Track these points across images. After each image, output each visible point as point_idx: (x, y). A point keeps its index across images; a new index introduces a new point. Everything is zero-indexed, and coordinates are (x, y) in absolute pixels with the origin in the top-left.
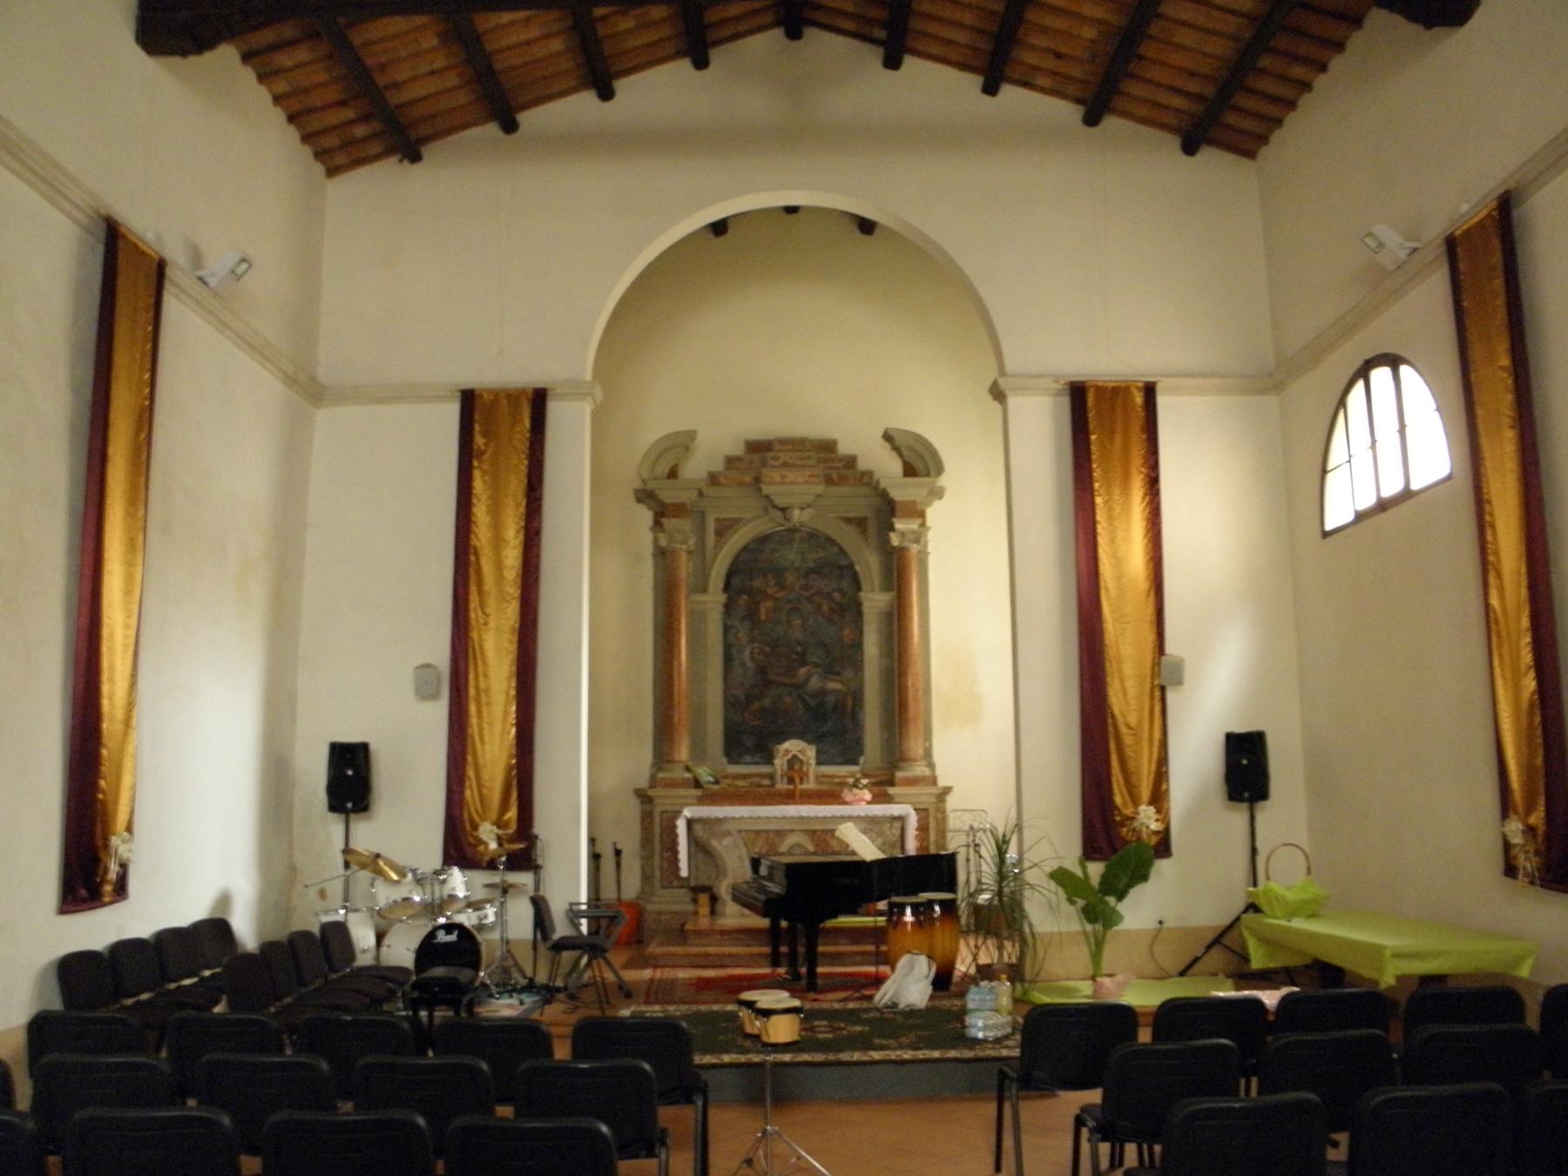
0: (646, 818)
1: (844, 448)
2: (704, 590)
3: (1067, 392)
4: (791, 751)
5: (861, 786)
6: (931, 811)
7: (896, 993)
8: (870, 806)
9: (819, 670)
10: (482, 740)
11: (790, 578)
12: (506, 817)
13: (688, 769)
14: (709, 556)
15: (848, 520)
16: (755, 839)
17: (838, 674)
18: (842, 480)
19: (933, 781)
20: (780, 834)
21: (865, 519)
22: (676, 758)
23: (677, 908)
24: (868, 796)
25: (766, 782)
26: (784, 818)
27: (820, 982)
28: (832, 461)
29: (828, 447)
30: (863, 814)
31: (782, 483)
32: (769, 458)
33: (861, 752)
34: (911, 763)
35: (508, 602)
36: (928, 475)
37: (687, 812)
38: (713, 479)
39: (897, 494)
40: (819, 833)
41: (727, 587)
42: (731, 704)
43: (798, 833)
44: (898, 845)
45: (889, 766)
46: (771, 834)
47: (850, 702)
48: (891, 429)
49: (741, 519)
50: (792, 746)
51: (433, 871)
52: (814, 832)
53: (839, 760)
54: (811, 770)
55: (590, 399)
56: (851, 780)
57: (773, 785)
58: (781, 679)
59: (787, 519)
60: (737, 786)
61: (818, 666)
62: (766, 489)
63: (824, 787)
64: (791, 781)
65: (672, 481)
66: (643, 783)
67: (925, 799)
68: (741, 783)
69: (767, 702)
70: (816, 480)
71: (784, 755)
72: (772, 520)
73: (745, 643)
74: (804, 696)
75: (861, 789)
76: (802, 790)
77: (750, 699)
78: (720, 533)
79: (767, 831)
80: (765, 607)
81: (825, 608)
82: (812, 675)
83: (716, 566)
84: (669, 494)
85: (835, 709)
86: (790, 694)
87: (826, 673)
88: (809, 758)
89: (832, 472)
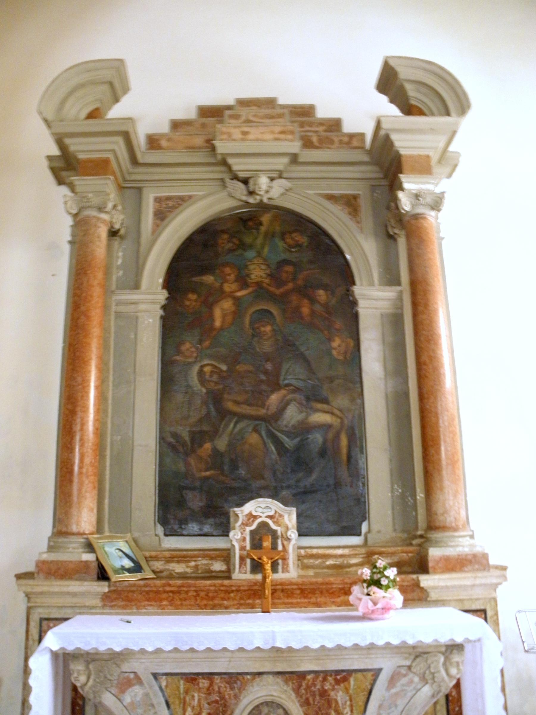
2: (137, 286)
4: (255, 517)
5: (384, 582)
9: (297, 396)
13: (90, 547)
14: (143, 249)
15: (331, 198)
16: (187, 692)
17: (325, 401)
28: (310, 124)
30: (395, 642)
33: (364, 516)
34: (447, 534)
40: (309, 677)
43: (270, 678)
45: (405, 535)
46: (217, 680)
47: (344, 441)
49: (190, 197)
52: (302, 675)
53: (332, 528)
54: (291, 549)
57: (227, 574)
61: (297, 390)
64: (257, 567)
68: (179, 568)
69: (222, 444)
71: (245, 524)
75: (388, 587)
76: (274, 584)
79: (210, 676)
82: (288, 404)
85: (323, 453)
86: (256, 430)
87: (308, 399)
88: (287, 529)
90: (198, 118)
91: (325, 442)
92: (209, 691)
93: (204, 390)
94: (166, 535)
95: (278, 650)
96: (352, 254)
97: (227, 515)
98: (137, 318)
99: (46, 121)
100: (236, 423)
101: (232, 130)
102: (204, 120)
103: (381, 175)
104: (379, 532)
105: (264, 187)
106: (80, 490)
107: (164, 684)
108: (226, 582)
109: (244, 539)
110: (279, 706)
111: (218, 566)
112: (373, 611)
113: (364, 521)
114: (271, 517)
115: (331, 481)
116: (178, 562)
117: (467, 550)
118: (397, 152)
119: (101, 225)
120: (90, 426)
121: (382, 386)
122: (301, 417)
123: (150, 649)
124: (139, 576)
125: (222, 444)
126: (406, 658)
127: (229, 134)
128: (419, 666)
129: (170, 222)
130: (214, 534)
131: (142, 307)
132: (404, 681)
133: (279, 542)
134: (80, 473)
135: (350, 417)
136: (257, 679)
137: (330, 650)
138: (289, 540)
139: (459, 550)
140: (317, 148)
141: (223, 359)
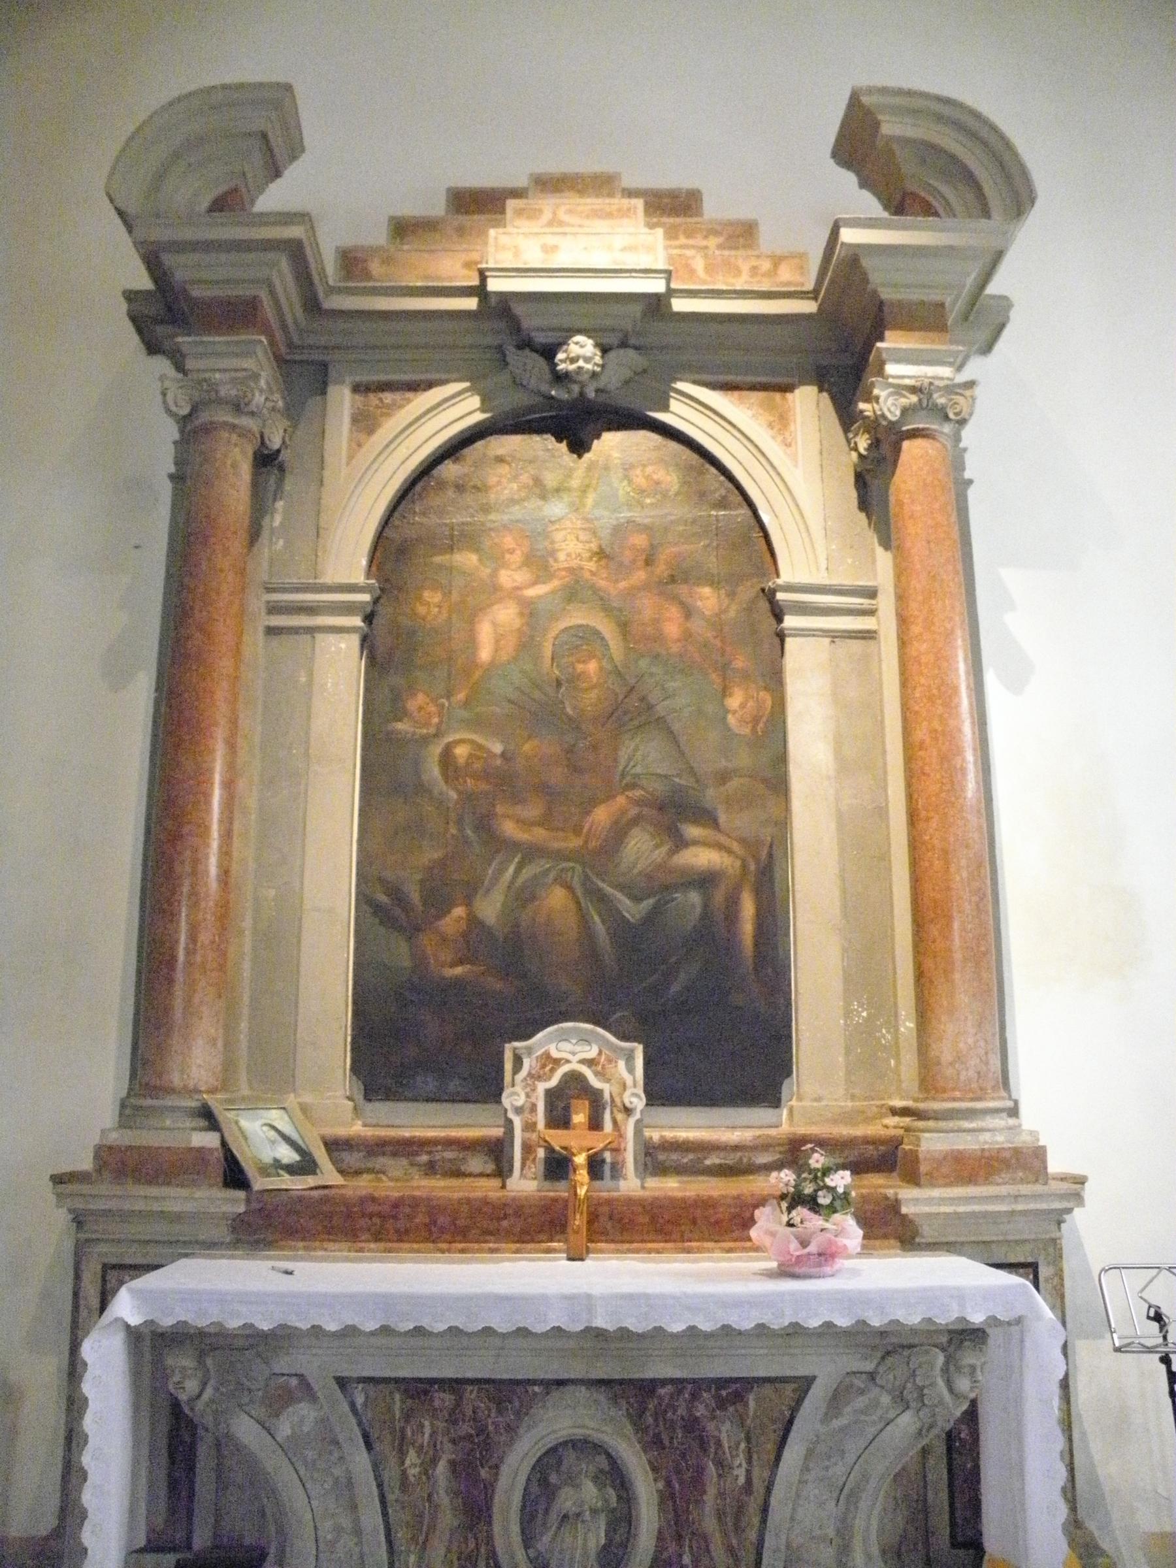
4: (557, 1062)
5: (824, 1199)
16: (407, 1416)
22: (176, 1080)
33: (783, 1068)
43: (582, 1392)
46: (471, 1393)
52: (648, 1387)
72: (517, 384)
75: (832, 1209)
79: (455, 1385)
90: (447, 212)
106: (188, 1001)
107: (360, 1400)
109: (533, 1108)
110: (598, 1448)
114: (590, 1063)
125: (490, 908)
132: (860, 1402)
136: (556, 1394)
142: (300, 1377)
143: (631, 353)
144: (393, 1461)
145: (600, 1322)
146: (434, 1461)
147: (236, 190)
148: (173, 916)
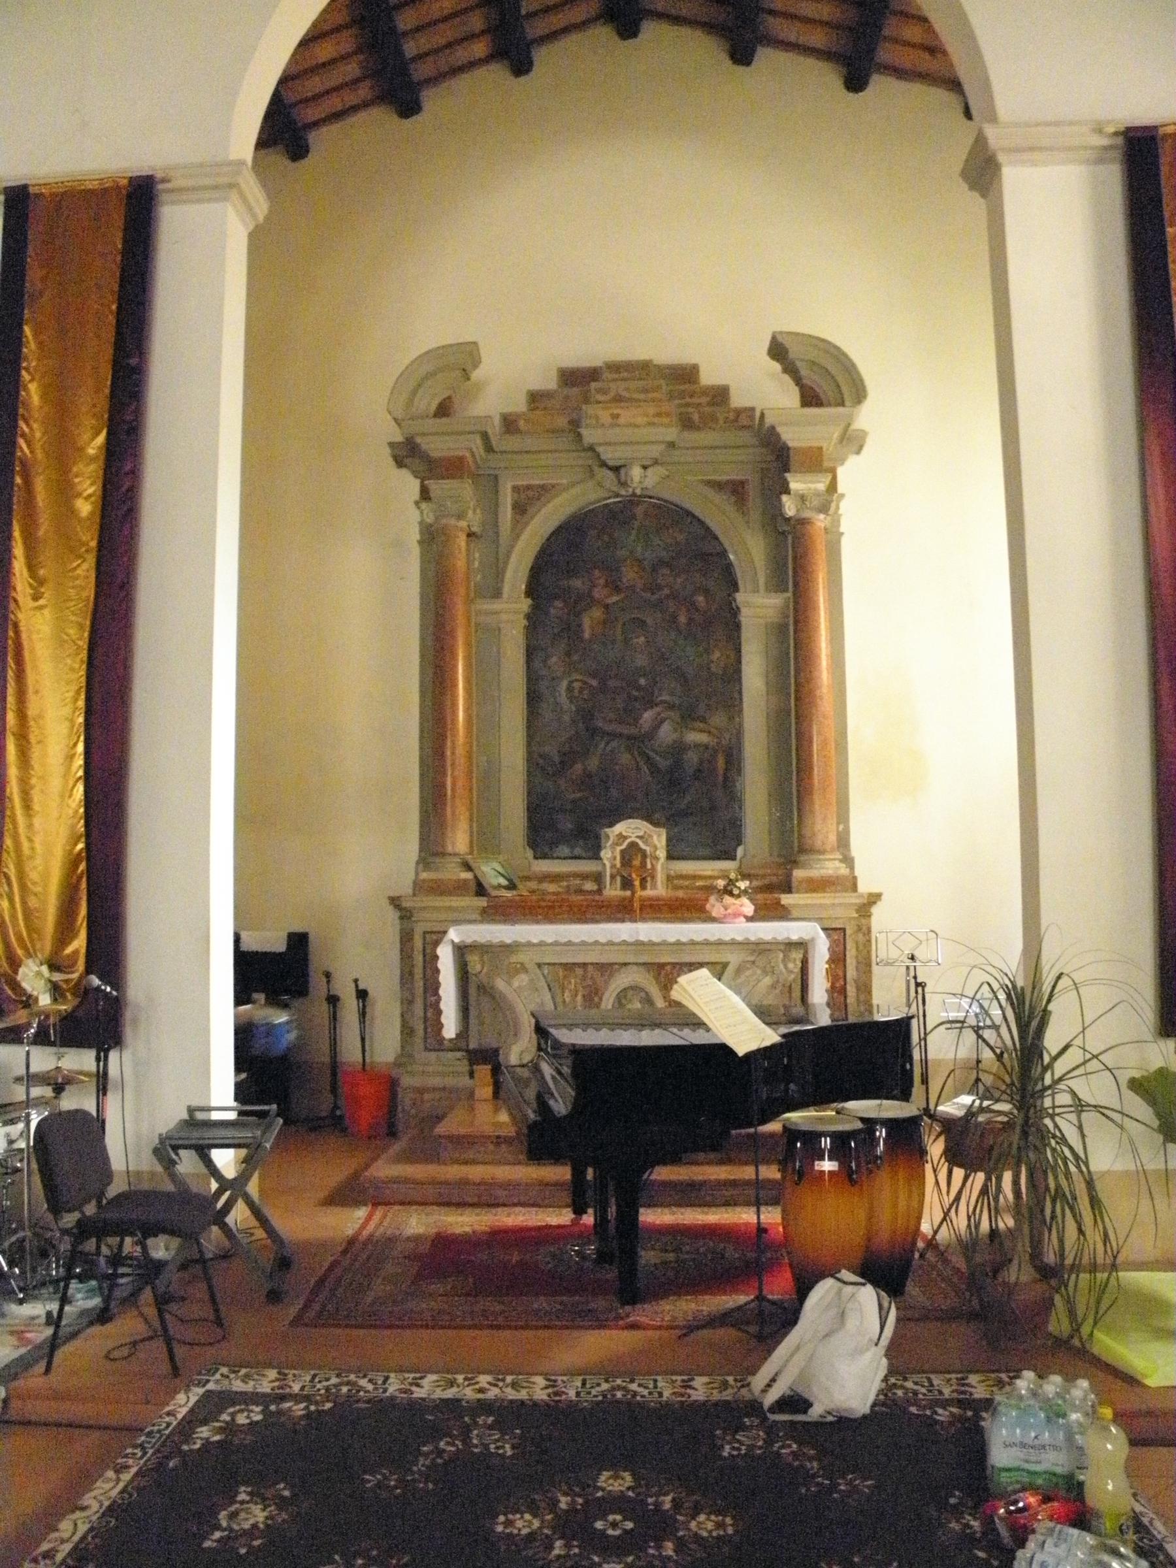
0: (406, 938)
1: (709, 377)
2: (497, 594)
3: (1117, 155)
4: (625, 838)
5: (736, 892)
6: (848, 932)
7: (803, 1375)
8: (751, 924)
10: (27, 806)
11: (629, 575)
12: (69, 950)
13: (468, 867)
14: (502, 550)
15: (719, 486)
16: (565, 977)
17: (703, 720)
18: (708, 422)
19: (852, 884)
20: (607, 969)
21: (742, 483)
23: (450, 1081)
24: (748, 908)
25: (589, 886)
26: (610, 943)
27: (648, 1257)
29: (685, 375)
30: (739, 938)
31: (613, 426)
32: (593, 391)
34: (812, 857)
35: (79, 557)
36: (842, 404)
37: (454, 935)
38: (510, 424)
39: (792, 436)
40: (668, 968)
41: (530, 592)
42: (536, 764)
43: (635, 968)
44: (797, 993)
46: (590, 968)
47: (721, 762)
48: (781, 332)
50: (629, 829)
51: (331, 970)
52: (661, 966)
53: (703, 852)
55: (234, 195)
56: (721, 883)
57: (599, 891)
58: (609, 728)
59: (623, 484)
60: (544, 893)
61: (672, 707)
62: (589, 435)
63: (680, 894)
64: (627, 884)
65: (444, 420)
66: (404, 886)
67: (840, 912)
68: (552, 888)
69: (593, 763)
70: (666, 420)
72: (600, 484)
73: (559, 674)
74: (651, 754)
75: (739, 896)
76: (642, 899)
77: (568, 758)
78: (520, 509)
79: (585, 965)
80: (589, 621)
81: (683, 619)
82: (662, 722)
83: (514, 559)
84: (437, 447)
85: (698, 773)
87: (682, 718)
88: (656, 848)
89: (690, 410)
90: (560, 387)
91: (701, 762)
92: (584, 978)
93: (574, 709)
94: (536, 858)
95: (642, 943)
96: (735, 553)
97: (598, 837)
98: (499, 629)
99: (396, 420)
100: (608, 743)
101: (600, 413)
102: (566, 391)
103: (773, 458)
104: (754, 856)
105: (636, 479)
106: (453, 813)
107: (546, 972)
108: (597, 897)
109: (615, 858)
110: (642, 990)
111: (589, 886)
112: (725, 916)
113: (739, 845)
114: (640, 837)
115: (705, 804)
116: (552, 882)
117: (830, 872)
118: (784, 443)
119: (460, 534)
120: (460, 751)
121: (763, 703)
122: (675, 736)
123: (535, 941)
124: (515, 892)
125: (593, 763)
126: (752, 954)
127: (597, 418)
128: (761, 961)
129: (532, 518)
130: (584, 855)
131: (504, 617)
132: (748, 973)
133: (648, 861)
134: (453, 797)
135: (727, 736)
136: (623, 969)
137: (684, 944)
138: (657, 859)
139: (823, 872)
140: (698, 429)
141: (594, 675)
142: (522, 964)
143: (659, 468)
144: (560, 995)
145: (641, 938)
146: (576, 995)
147: (449, 398)
148: (444, 774)
